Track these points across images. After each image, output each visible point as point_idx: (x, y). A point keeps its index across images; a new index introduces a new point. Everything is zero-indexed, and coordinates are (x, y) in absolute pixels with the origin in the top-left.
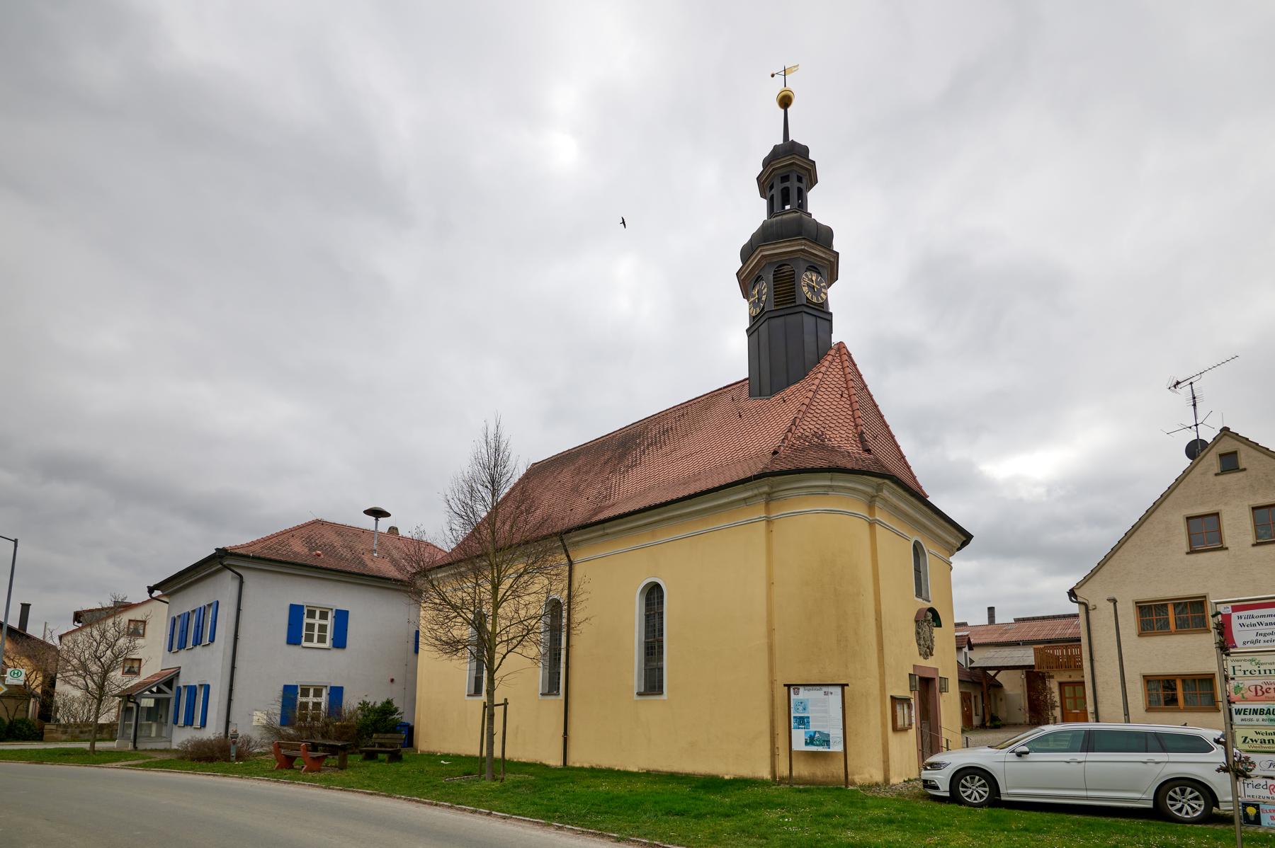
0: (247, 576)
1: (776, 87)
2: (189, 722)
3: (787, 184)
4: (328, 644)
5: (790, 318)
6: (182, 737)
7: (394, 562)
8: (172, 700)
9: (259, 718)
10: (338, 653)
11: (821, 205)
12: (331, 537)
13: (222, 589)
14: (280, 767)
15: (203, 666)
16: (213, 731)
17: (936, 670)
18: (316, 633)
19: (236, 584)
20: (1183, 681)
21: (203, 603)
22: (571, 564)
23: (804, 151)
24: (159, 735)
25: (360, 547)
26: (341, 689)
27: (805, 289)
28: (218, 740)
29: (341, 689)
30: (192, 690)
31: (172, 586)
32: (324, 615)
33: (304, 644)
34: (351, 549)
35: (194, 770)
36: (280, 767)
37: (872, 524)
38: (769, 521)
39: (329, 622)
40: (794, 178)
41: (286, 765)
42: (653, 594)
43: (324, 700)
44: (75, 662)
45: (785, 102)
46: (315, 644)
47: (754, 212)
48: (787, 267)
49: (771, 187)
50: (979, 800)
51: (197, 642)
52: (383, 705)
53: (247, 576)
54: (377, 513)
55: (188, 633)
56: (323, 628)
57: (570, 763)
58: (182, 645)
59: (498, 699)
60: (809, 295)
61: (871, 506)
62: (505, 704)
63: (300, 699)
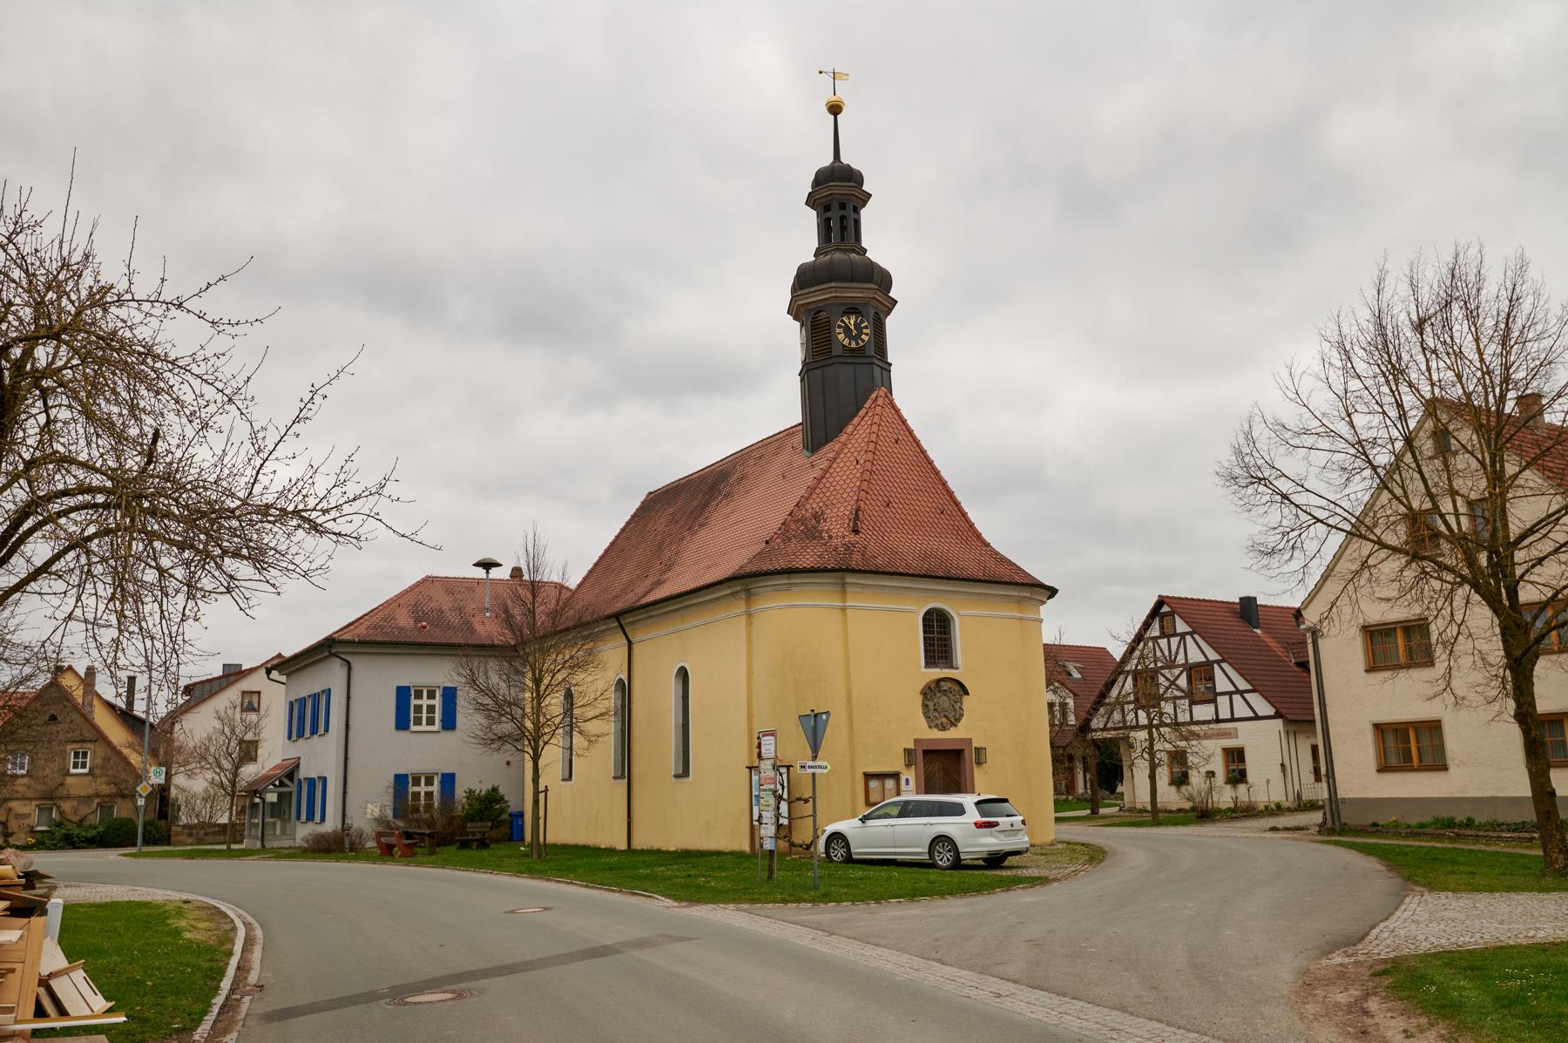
0: (353, 660)
1: (828, 97)
2: (310, 817)
3: (829, 214)
4: (437, 726)
6: (304, 832)
8: (291, 792)
9: (373, 810)
10: (448, 736)
11: (880, 239)
12: (442, 600)
13: (330, 677)
14: (382, 854)
15: (320, 758)
16: (331, 824)
17: (970, 740)
18: (424, 715)
19: (344, 671)
20: (1416, 730)
21: (317, 689)
22: (630, 643)
24: (283, 832)
25: (471, 606)
26: (453, 775)
27: (841, 337)
28: (335, 832)
29: (453, 775)
30: (311, 782)
31: (286, 666)
32: (431, 695)
33: (414, 728)
34: (460, 610)
35: (315, 859)
36: (382, 854)
38: (749, 615)
39: (437, 702)
40: (835, 207)
41: (387, 852)
42: (683, 674)
43: (435, 788)
44: (211, 759)
45: (835, 109)
46: (424, 727)
47: (801, 240)
51: (314, 731)
52: (488, 793)
53: (353, 660)
54: (487, 565)
55: (307, 718)
56: (431, 709)
57: (634, 846)
58: (301, 735)
59: (542, 788)
60: (846, 342)
62: (546, 790)
63: (412, 789)
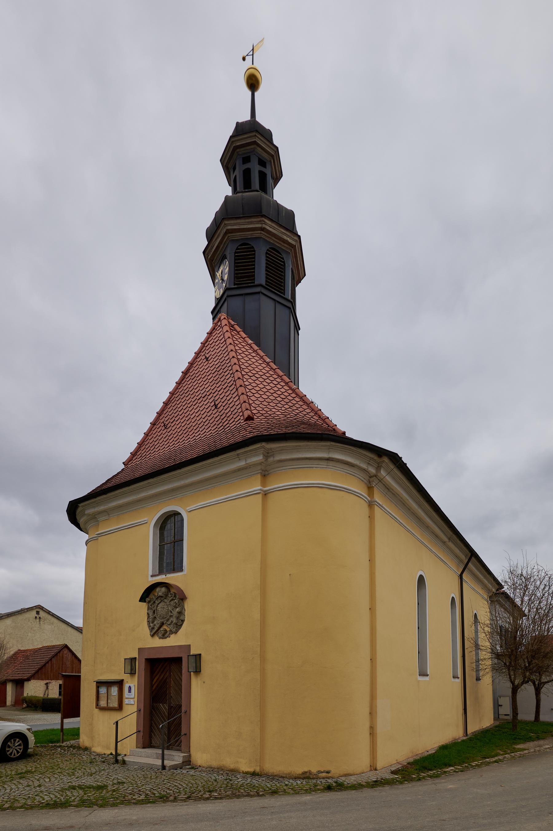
5: (248, 299)
7: (495, 607)
23: (267, 135)
37: (371, 505)
45: (253, 83)
48: (255, 254)
49: (234, 169)
50: (17, 755)
61: (370, 489)
